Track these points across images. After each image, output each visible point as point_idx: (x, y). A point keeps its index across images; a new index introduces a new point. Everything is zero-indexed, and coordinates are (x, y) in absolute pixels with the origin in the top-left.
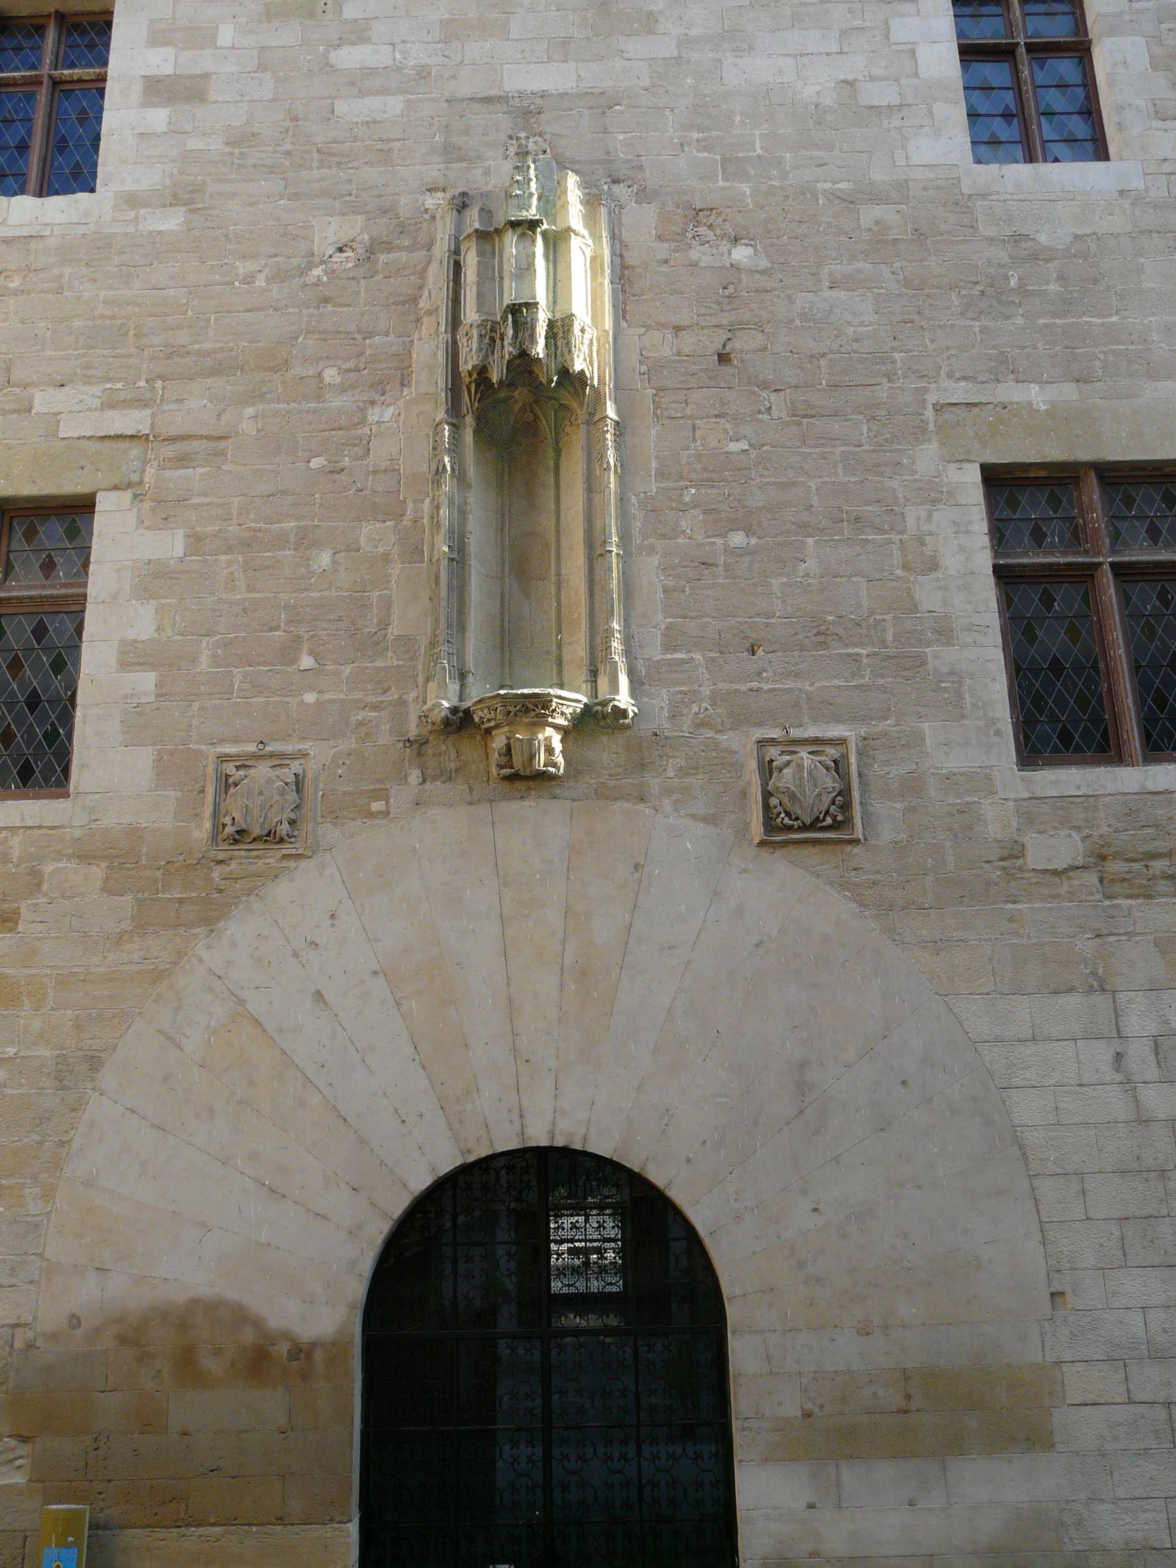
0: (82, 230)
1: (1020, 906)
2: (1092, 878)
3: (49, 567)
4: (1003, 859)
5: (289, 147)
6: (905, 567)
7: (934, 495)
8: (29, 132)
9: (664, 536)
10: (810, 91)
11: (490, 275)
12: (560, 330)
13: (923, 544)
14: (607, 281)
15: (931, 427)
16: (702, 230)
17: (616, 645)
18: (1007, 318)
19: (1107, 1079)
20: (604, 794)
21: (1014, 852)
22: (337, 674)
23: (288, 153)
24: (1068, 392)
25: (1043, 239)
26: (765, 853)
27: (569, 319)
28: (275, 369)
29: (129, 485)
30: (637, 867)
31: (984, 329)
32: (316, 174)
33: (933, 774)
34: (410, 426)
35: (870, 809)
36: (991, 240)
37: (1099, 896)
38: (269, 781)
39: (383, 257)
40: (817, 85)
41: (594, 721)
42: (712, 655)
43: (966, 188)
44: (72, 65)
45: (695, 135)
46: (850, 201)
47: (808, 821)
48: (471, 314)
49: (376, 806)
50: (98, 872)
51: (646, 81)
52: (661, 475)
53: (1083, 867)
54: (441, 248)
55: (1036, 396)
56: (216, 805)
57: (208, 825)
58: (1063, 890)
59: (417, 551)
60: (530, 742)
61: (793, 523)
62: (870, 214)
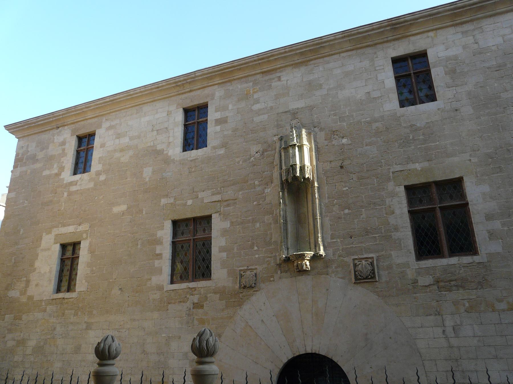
0: (205, 156)
2: (435, 287)
3: (204, 230)
4: (412, 283)
5: (244, 130)
6: (386, 214)
7: (393, 195)
8: (194, 135)
9: (330, 212)
10: (359, 96)
11: (287, 157)
12: (302, 168)
13: (390, 208)
14: (314, 153)
15: (391, 178)
16: (335, 136)
17: (320, 240)
18: (410, 147)
19: (441, 337)
20: (320, 274)
21: (415, 282)
22: (262, 250)
23: (245, 132)
24: (426, 164)
25: (418, 125)
26: (355, 285)
27: (304, 166)
28: (245, 183)
29: (218, 212)
30: (327, 290)
31: (404, 151)
32: (251, 136)
34: (273, 193)
36: (405, 127)
37: (437, 291)
38: (250, 275)
39: (265, 153)
40: (361, 95)
41: (316, 258)
43: (398, 115)
44: (201, 118)
45: (332, 113)
46: (369, 123)
48: (284, 167)
49: (272, 279)
50: (218, 296)
51: (320, 101)
52: (329, 198)
53: (433, 284)
54: (277, 150)
55: (418, 166)
56: (240, 281)
57: (238, 285)
58: (428, 291)
59: (277, 221)
60: (302, 263)
62: (375, 125)
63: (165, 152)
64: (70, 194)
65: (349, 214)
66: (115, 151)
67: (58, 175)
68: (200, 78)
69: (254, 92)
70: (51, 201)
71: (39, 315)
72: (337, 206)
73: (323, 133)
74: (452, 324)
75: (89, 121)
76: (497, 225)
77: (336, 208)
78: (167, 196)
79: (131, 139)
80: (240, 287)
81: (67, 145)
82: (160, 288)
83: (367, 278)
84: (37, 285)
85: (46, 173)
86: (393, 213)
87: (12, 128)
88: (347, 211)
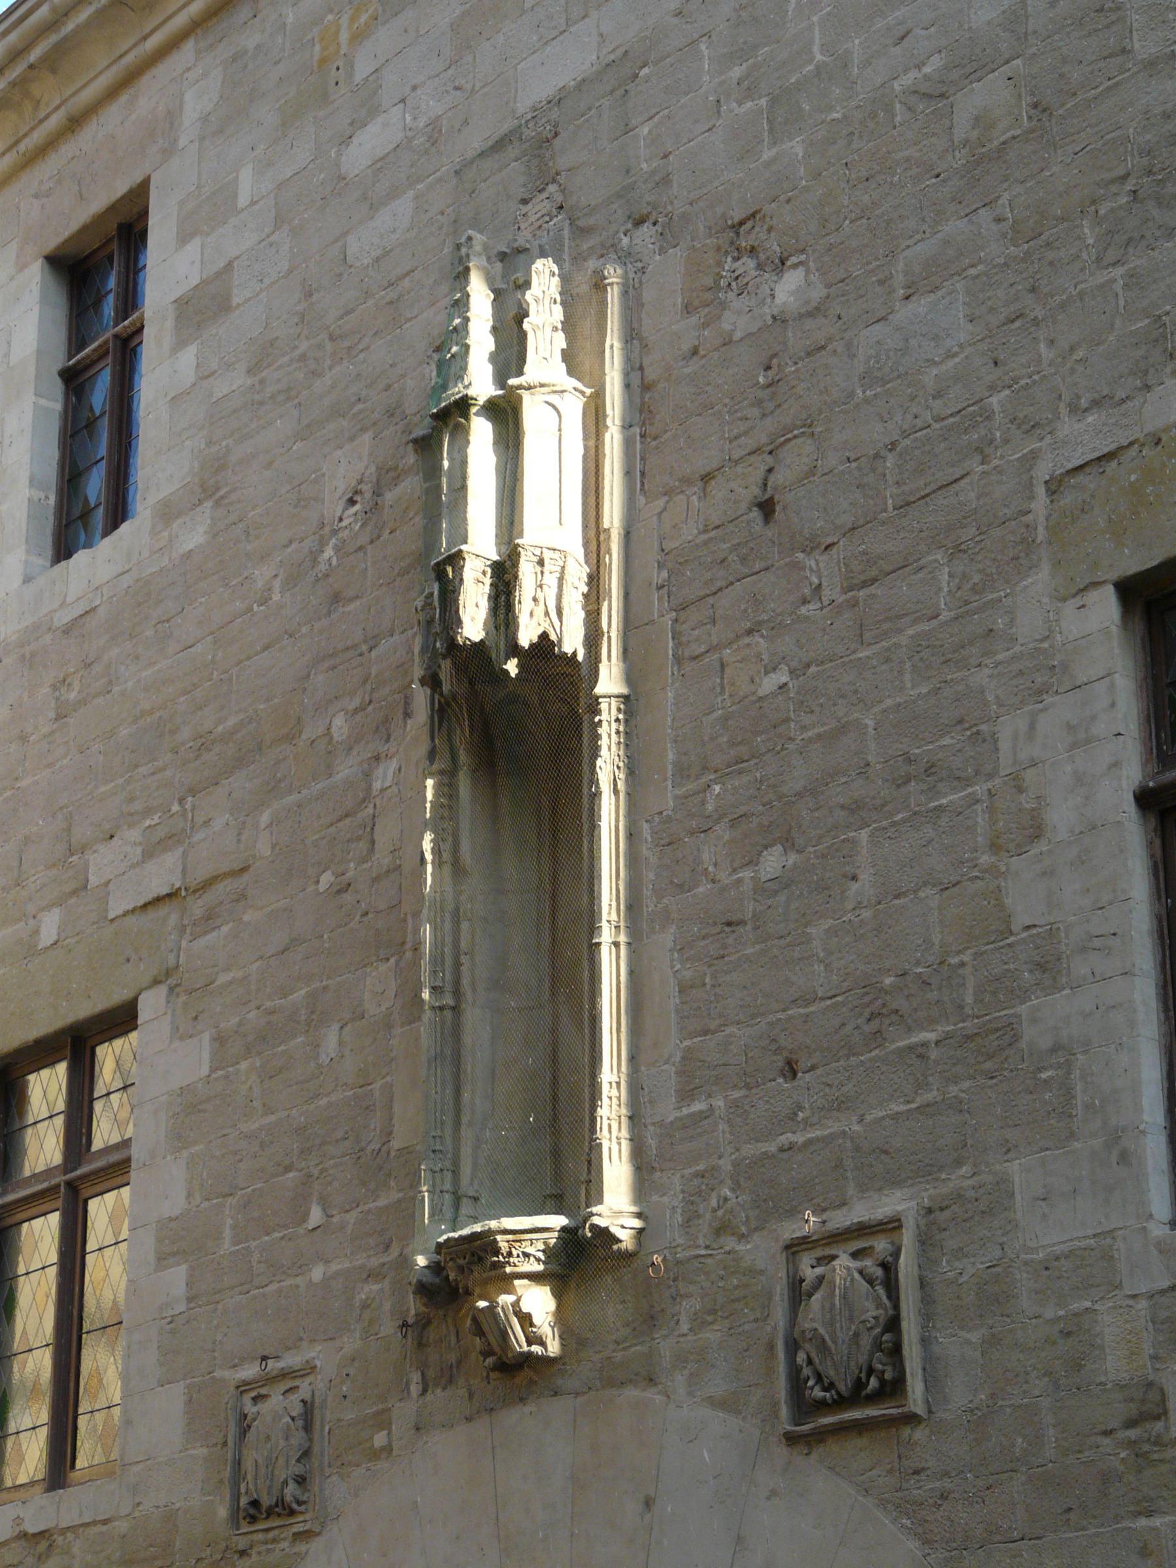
0: (126, 581)
1: (1157, 1522)
4: (1131, 1424)
15: (1041, 534)
30: (648, 1503)
33: (1026, 1263)
34: (418, 797)
35: (936, 1349)
42: (737, 1094)
46: (937, 95)
47: (843, 1387)
49: (380, 1439)
52: (682, 772)
60: (492, 1308)
61: (842, 807)
65: (783, 883)
72: (723, 832)
80: (235, 1517)
86: (1036, 830)
88: (773, 862)
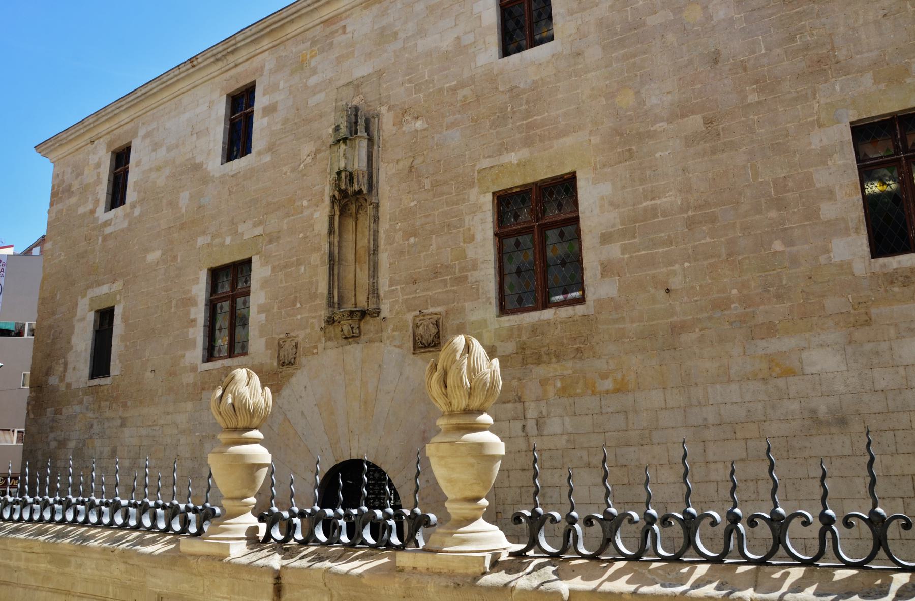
25: (521, 86)
31: (497, 133)
36: (503, 92)
40: (447, 43)
46: (454, 90)
49: (315, 351)
62: (461, 93)
63: (205, 166)
64: (105, 239)
66: (151, 170)
67: (93, 212)
68: (243, 43)
69: (312, 57)
70: (86, 252)
71: (77, 408)
73: (392, 113)
74: (536, 415)
75: (125, 128)
76: (614, 251)
77: (399, 236)
78: (204, 233)
79: (169, 150)
81: (102, 166)
82: (194, 369)
83: (429, 346)
84: (74, 368)
85: (81, 210)
87: (43, 148)
